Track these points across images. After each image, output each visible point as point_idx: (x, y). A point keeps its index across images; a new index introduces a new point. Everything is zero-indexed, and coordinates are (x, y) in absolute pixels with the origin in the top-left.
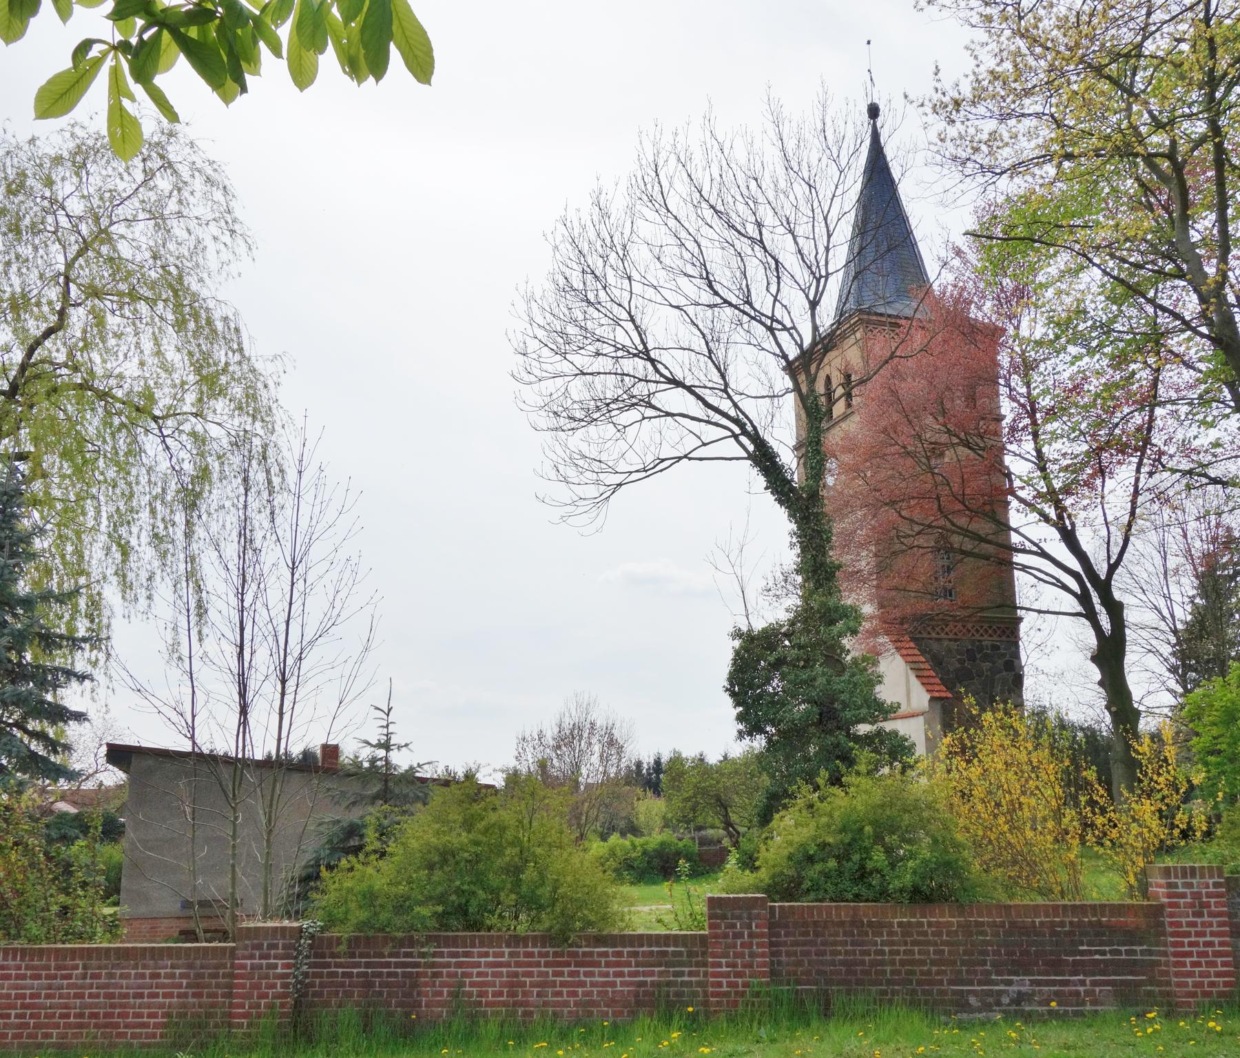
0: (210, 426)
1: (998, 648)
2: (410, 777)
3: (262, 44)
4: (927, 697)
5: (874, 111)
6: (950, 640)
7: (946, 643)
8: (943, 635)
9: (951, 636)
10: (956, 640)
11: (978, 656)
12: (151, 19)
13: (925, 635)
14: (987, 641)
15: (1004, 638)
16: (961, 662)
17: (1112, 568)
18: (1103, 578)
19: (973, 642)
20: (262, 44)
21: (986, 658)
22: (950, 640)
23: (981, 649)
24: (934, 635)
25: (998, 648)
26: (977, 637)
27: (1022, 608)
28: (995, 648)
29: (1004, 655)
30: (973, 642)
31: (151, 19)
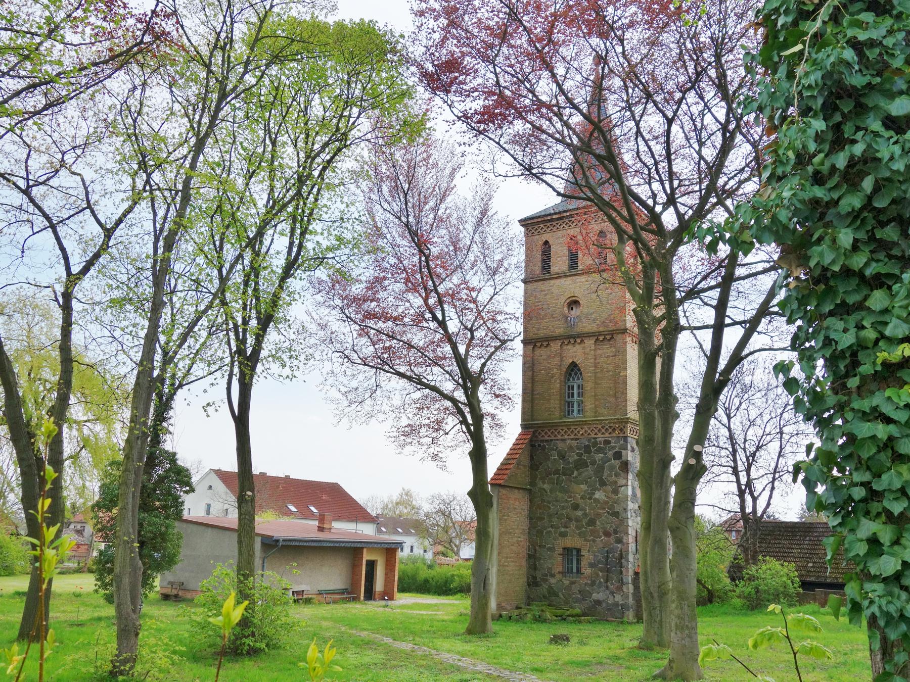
0: (237, 35)
1: (609, 442)
2: (268, 326)
5: (208, 416)
6: (572, 439)
7: (568, 442)
8: (566, 437)
9: (572, 436)
10: (577, 439)
13: (553, 438)
14: (601, 438)
16: (580, 455)
18: (719, 290)
19: (589, 440)
21: (600, 450)
22: (572, 439)
23: (595, 444)
24: (559, 437)
27: (718, 121)
29: (614, 448)
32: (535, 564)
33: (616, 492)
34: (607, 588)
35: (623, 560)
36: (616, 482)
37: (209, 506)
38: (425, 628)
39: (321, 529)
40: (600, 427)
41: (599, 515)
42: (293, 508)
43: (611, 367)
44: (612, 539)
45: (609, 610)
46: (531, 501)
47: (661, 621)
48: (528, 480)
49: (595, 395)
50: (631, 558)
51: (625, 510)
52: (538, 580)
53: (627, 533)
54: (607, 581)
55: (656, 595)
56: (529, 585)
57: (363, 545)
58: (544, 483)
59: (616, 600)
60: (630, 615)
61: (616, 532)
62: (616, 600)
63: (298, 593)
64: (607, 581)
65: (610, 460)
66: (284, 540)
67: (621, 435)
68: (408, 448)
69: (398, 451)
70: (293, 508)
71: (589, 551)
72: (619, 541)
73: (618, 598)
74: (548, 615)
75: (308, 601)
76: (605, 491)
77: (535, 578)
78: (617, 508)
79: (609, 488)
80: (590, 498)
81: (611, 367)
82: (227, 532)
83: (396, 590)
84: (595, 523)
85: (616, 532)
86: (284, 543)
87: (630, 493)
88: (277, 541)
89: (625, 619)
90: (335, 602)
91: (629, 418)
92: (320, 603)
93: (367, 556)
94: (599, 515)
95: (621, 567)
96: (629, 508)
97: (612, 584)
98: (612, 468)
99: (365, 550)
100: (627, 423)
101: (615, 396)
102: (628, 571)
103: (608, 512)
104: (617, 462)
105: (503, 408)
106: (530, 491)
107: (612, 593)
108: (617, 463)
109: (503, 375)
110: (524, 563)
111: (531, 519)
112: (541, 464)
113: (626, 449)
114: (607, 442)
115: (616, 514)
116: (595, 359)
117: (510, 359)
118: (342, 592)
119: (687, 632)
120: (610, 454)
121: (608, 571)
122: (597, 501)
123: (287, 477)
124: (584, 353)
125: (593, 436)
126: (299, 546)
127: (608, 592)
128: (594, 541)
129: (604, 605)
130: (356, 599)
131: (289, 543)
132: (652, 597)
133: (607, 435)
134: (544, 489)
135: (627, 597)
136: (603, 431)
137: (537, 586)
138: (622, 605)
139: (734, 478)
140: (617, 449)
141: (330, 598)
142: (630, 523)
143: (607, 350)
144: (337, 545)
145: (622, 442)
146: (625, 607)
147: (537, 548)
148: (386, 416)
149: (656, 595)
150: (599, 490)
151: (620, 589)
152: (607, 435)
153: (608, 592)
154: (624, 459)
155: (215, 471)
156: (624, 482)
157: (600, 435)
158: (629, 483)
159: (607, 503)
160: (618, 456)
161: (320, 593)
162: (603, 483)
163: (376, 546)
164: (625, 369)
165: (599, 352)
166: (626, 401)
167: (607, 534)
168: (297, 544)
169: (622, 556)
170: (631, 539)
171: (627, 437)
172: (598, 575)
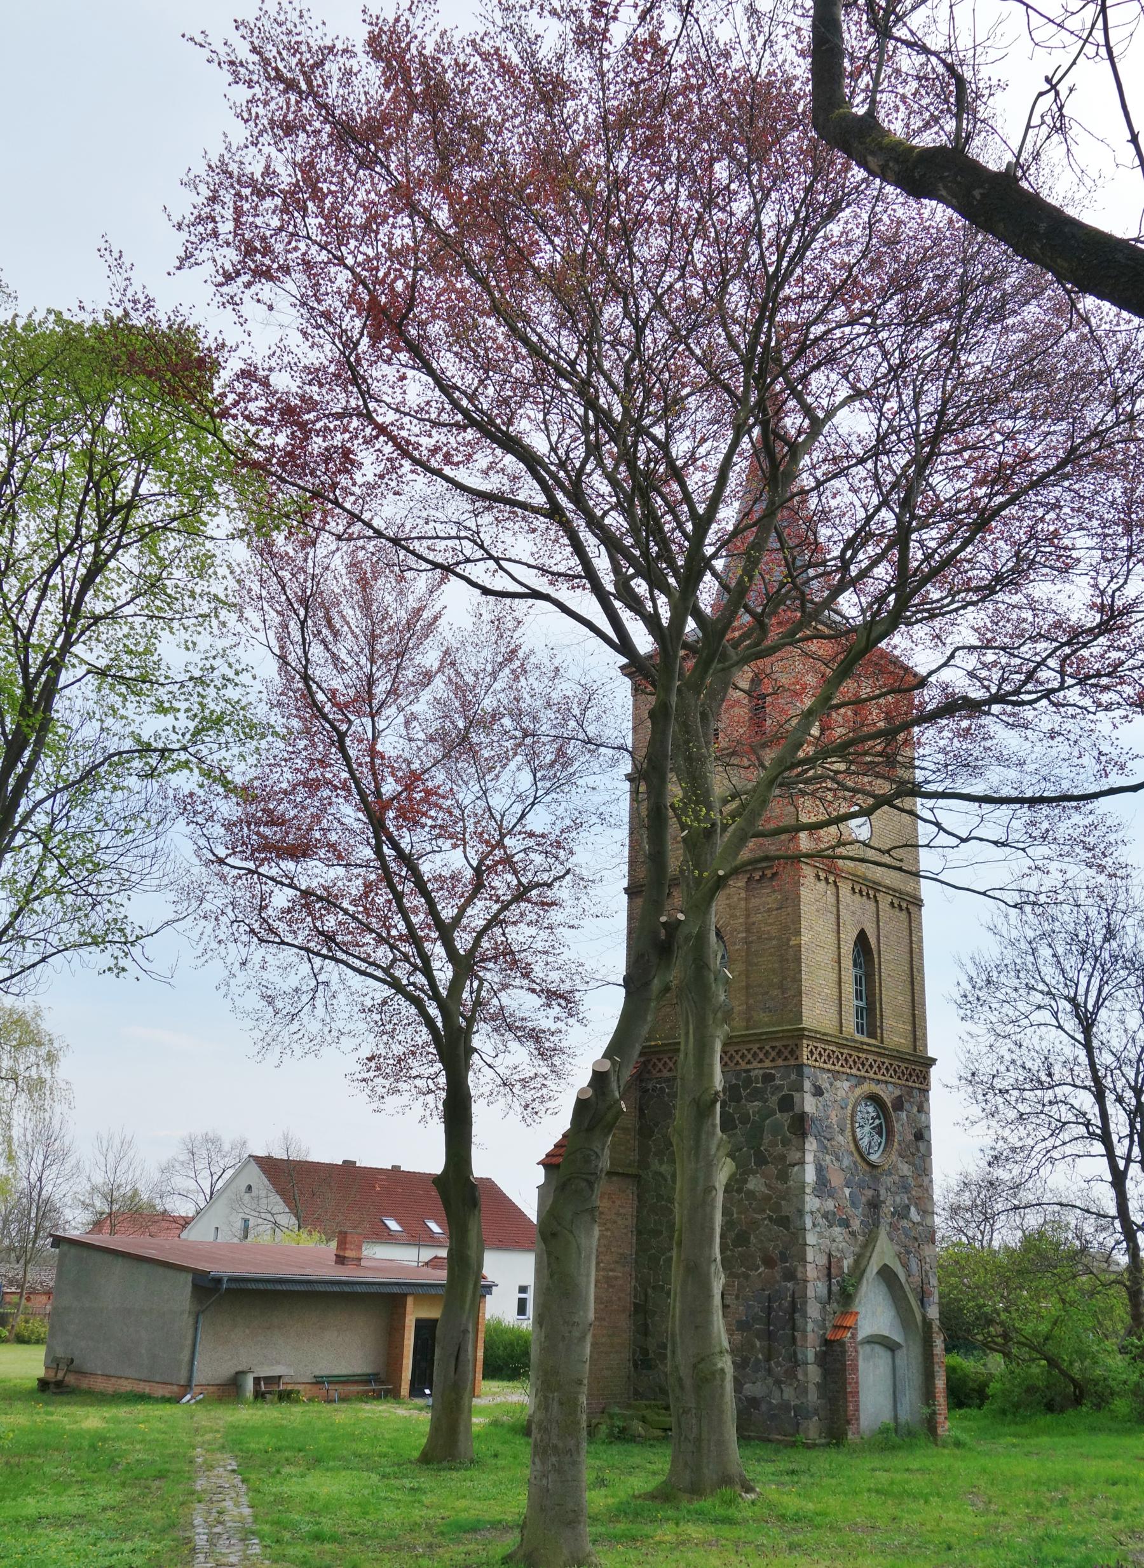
21: (756, 1095)
23: (748, 1081)
29: (779, 1088)
32: (646, 1325)
33: (783, 1176)
34: (769, 1371)
35: (797, 1316)
36: (783, 1157)
37: (246, 1221)
38: (364, 1448)
39: (341, 1260)
40: (755, 1047)
41: (755, 1224)
42: (393, 1225)
43: (774, 931)
44: (777, 1273)
45: (773, 1417)
46: (640, 1198)
47: (699, 1440)
48: (635, 1156)
49: (748, 987)
50: (813, 1310)
51: (801, 1213)
52: (651, 1355)
53: (804, 1260)
54: (768, 1359)
55: (688, 1383)
56: (635, 1366)
57: (405, 1290)
58: (661, 1162)
59: (786, 1396)
60: (813, 1428)
61: (784, 1258)
62: (786, 1396)
63: (269, 1380)
64: (768, 1359)
65: (773, 1113)
66: (231, 1280)
67: (793, 1062)
68: (392, 1101)
69: (374, 1106)
70: (393, 1225)
71: (737, 1297)
72: (790, 1275)
73: (789, 1393)
74: (639, 1428)
75: (286, 1396)
76: (764, 1176)
77: (645, 1351)
78: (787, 1209)
79: (772, 1169)
80: (739, 1191)
81: (774, 931)
82: (146, 1266)
83: (479, 1376)
84: (747, 1240)
85: (784, 1258)
86: (234, 1286)
87: (810, 1175)
88: (218, 1280)
89: (801, 1437)
90: (344, 1399)
91: (804, 1029)
92: (311, 1400)
93: (413, 1314)
94: (755, 1224)
95: (794, 1329)
96: (808, 1208)
97: (778, 1364)
98: (776, 1129)
99: (410, 1301)
100: (802, 1037)
101: (782, 988)
102: (805, 1337)
103: (770, 1218)
104: (786, 1115)
105: (571, 1021)
106: (637, 1177)
107: (778, 1382)
108: (784, 1118)
109: (567, 955)
110: (624, 1322)
111: (639, 1233)
112: (656, 1125)
113: (801, 1089)
114: (768, 1078)
115: (784, 1222)
116: (748, 916)
117: (575, 922)
118: (366, 1379)
119: (554, 1459)
120: (773, 1101)
121: (770, 1336)
122: (751, 1194)
123: (396, 1169)
124: (729, 905)
125: (743, 1065)
126: (326, 1293)
127: (770, 1381)
128: (747, 1277)
129: (764, 1407)
130: (392, 1394)
131: (243, 1286)
132: (682, 1387)
133: (768, 1063)
134: (661, 1174)
135: (805, 1391)
136: (761, 1056)
137: (650, 1367)
138: (796, 1408)
139: (1099, 1148)
140: (785, 1092)
141: (335, 1391)
142: (811, 1238)
143: (767, 898)
144: (347, 1289)
145: (793, 1077)
146: (801, 1412)
147: (650, 1291)
148: (357, 1041)
149: (688, 1383)
150: (754, 1173)
151: (791, 1374)
152: (768, 1063)
153: (770, 1381)
154: (797, 1110)
155: (257, 1159)
156: (799, 1155)
157: (755, 1064)
158: (809, 1158)
159: (769, 1198)
160: (787, 1104)
161: (319, 1381)
162: (761, 1160)
163: (433, 1291)
164: (798, 933)
165: (755, 902)
166: (800, 993)
167: (769, 1262)
168: (261, 1286)
169: (796, 1306)
170: (811, 1272)
171: (802, 1065)
172: (753, 1346)
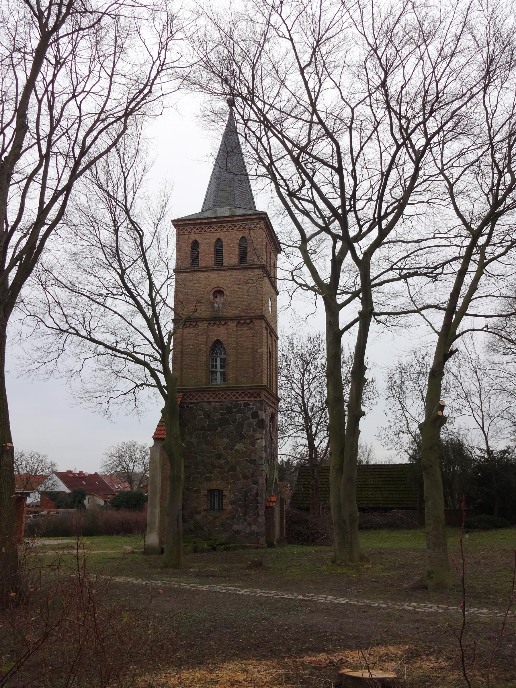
1: (248, 405)
3: (349, 252)
4: (279, 255)
6: (216, 402)
7: (213, 404)
8: (211, 400)
10: (220, 402)
11: (234, 410)
12: (476, 235)
13: (200, 400)
15: (252, 398)
16: (223, 414)
17: (96, 114)
19: (231, 402)
20: (349, 252)
21: (239, 411)
22: (216, 402)
24: (205, 400)
25: (248, 405)
26: (234, 399)
28: (246, 405)
29: (252, 409)
30: (231, 402)
31: (476, 235)
